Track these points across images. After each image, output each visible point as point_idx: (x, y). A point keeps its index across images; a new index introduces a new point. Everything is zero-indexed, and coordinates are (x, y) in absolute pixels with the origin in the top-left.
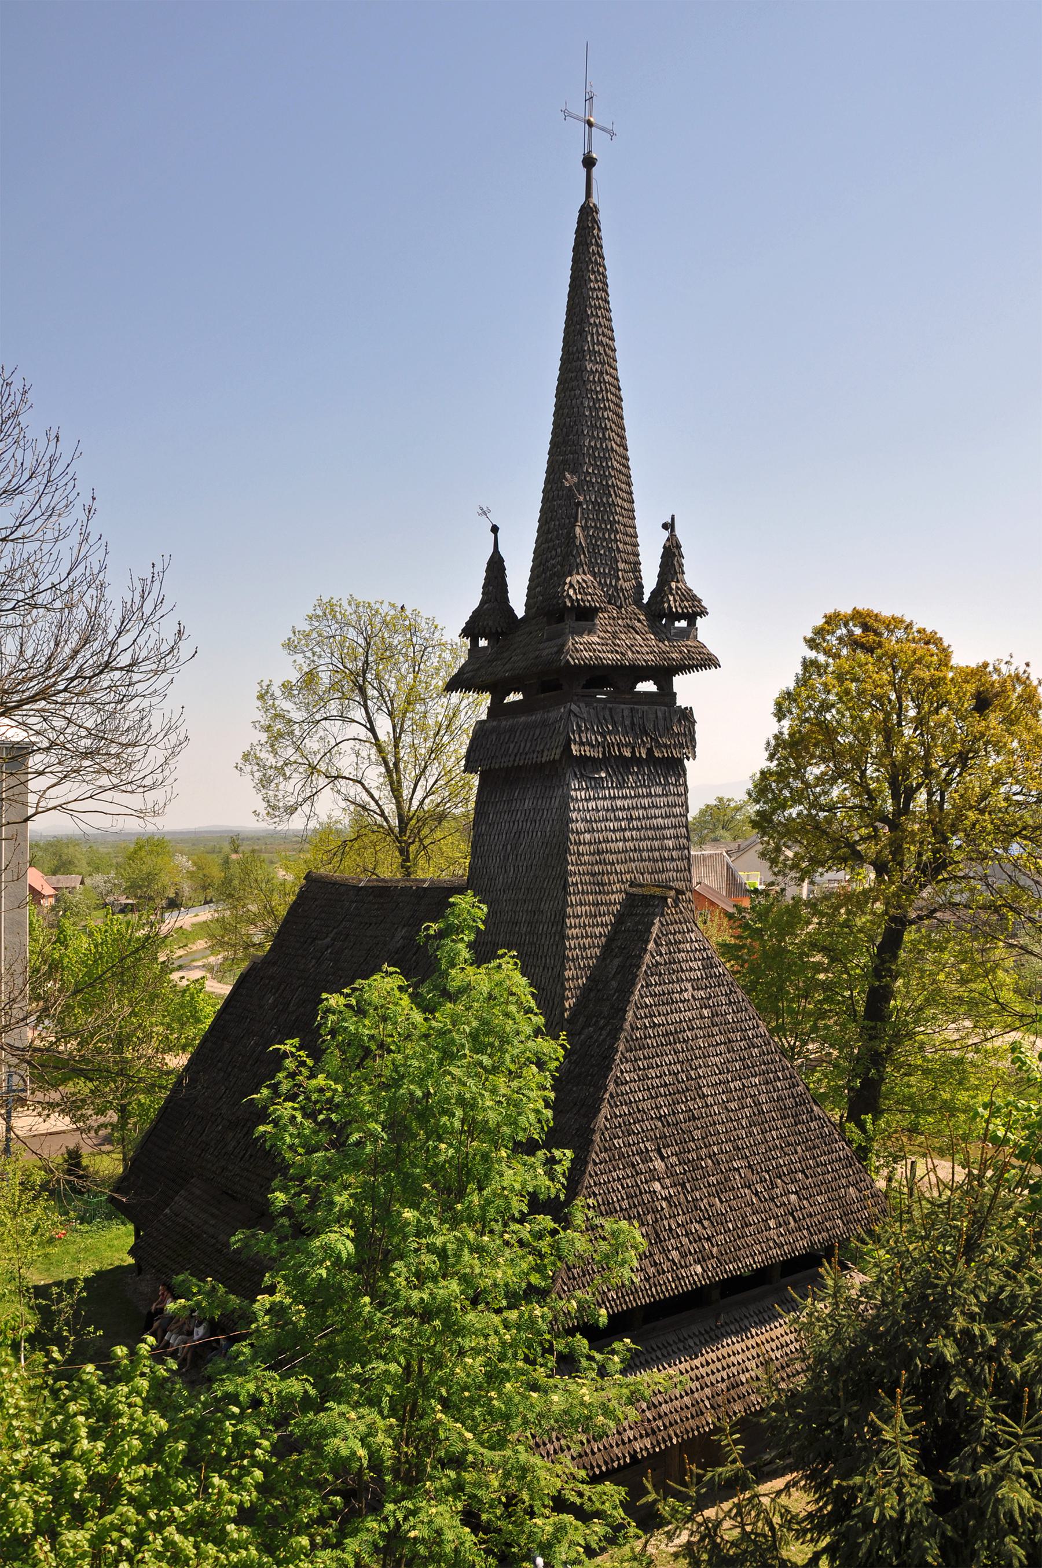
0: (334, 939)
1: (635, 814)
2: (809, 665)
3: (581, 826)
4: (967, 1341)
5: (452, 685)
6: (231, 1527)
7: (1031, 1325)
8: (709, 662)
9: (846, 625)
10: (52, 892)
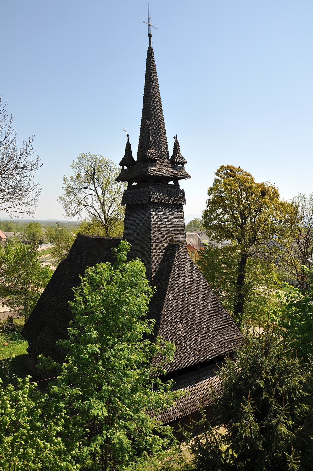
0: (86, 254)
1: (170, 220)
2: (216, 180)
3: (154, 222)
4: (267, 381)
5: (118, 179)
6: (54, 438)
7: (284, 376)
8: (188, 177)
9: (226, 169)
10: (5, 237)
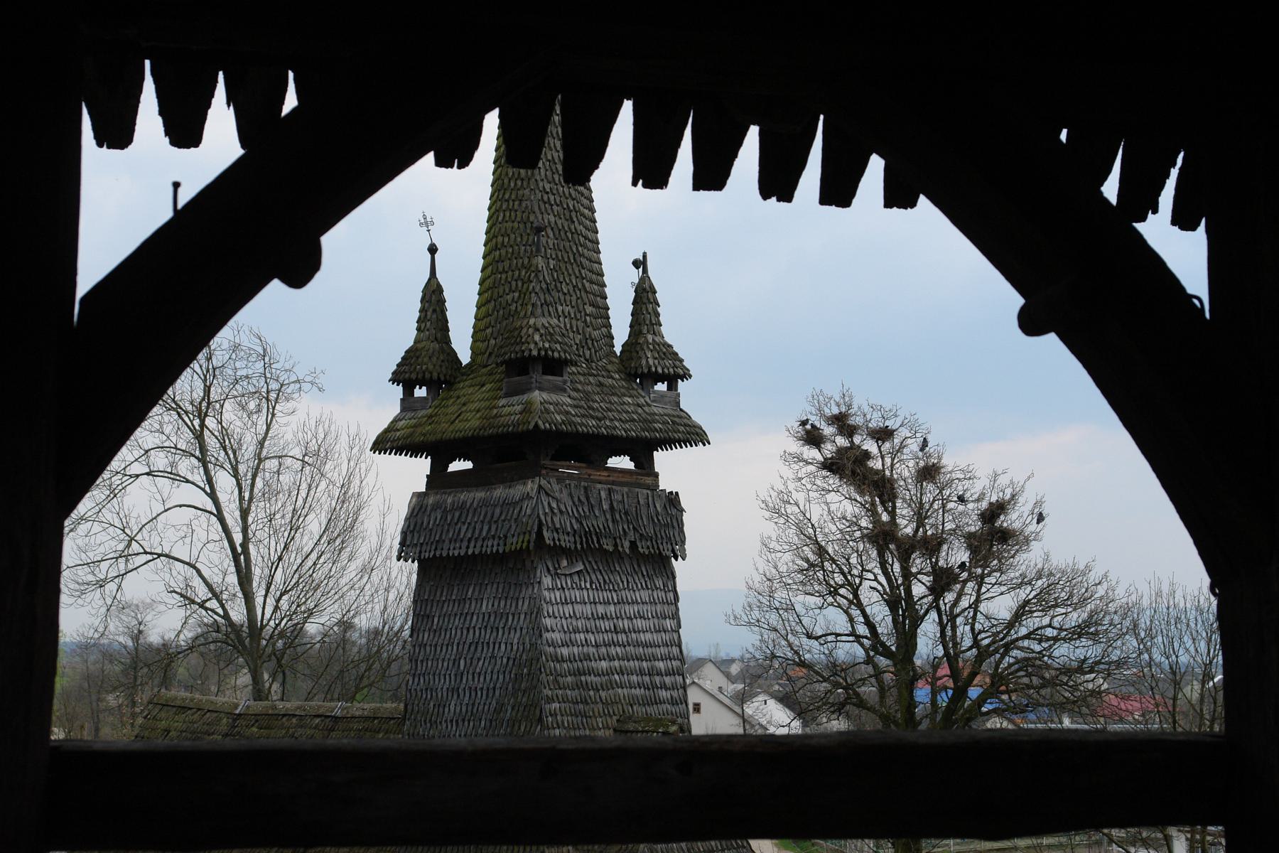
3: (556, 636)
8: (693, 435)
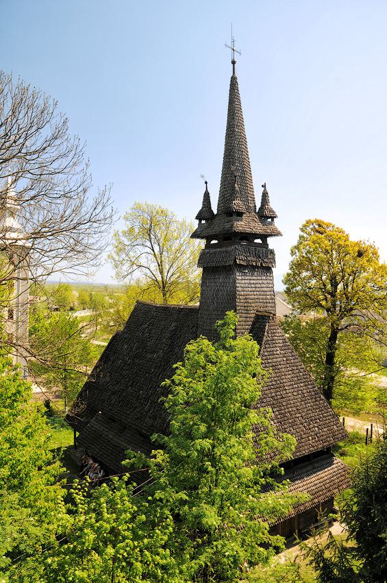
1: (257, 286)
2: (301, 237)
3: (240, 289)
